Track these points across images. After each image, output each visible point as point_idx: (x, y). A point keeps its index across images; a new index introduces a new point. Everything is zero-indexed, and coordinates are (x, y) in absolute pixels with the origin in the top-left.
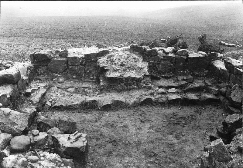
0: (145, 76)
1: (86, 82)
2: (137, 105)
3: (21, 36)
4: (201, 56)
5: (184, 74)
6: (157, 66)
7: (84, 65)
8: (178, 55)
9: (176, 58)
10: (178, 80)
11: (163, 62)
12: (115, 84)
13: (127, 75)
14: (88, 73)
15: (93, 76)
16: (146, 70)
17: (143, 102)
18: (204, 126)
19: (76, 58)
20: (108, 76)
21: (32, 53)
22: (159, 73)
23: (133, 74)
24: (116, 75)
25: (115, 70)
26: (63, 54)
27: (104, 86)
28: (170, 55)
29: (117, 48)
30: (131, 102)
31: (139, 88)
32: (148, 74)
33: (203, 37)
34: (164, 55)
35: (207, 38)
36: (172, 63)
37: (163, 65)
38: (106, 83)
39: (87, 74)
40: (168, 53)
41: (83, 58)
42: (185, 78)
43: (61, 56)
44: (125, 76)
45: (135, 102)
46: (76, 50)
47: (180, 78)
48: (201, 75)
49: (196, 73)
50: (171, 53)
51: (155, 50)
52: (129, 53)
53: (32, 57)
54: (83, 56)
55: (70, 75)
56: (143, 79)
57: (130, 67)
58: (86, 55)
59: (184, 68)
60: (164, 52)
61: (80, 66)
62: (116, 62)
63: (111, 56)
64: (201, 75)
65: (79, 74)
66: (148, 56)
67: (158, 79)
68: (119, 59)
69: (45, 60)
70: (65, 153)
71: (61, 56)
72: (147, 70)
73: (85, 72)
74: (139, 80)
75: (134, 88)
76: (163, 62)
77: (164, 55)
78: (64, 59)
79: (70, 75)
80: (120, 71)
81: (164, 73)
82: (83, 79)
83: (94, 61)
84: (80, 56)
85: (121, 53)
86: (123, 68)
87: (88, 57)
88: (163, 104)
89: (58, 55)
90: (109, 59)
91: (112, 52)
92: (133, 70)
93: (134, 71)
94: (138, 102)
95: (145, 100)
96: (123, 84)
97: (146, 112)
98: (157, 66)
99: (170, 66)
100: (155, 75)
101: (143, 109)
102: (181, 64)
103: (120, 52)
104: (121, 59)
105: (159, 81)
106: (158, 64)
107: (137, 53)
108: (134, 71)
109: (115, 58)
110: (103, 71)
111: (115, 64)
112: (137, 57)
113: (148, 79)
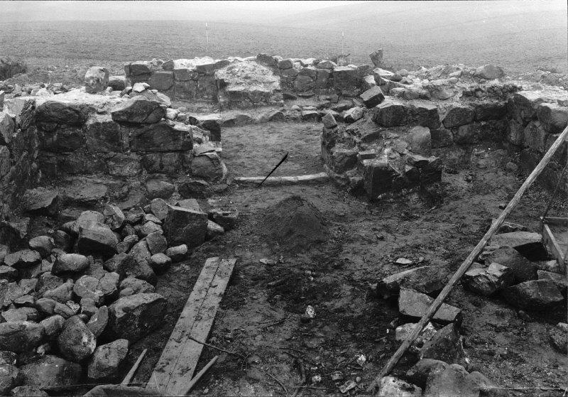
0: (277, 91)
1: (199, 102)
2: (264, 121)
3: (48, 56)
4: (350, 69)
5: (327, 93)
6: (292, 82)
7: (197, 81)
8: (320, 68)
9: (317, 72)
10: (319, 100)
11: (299, 77)
12: (236, 99)
13: (253, 88)
14: (201, 91)
15: (208, 94)
16: (277, 85)
17: (272, 117)
18: (428, 257)
19: (186, 70)
20: (230, 90)
21: (128, 63)
22: (294, 91)
23: (261, 88)
24: (240, 88)
25: (237, 84)
26: (167, 66)
27: (224, 102)
28: (309, 68)
29: (239, 59)
30: (258, 117)
31: (269, 104)
32: (279, 88)
33: (377, 54)
34: (302, 67)
35: (385, 55)
36: (312, 78)
37: (301, 81)
38: (227, 100)
39: (201, 93)
40: (307, 65)
41: (194, 71)
42: (328, 97)
43: (165, 68)
44: (251, 90)
45: (263, 117)
46: (185, 61)
47: (322, 97)
48: (351, 95)
49: (344, 92)
50: (312, 65)
51: (289, 62)
52: (255, 64)
53: (128, 70)
54: (195, 68)
55: (177, 94)
56: (273, 95)
57: (256, 81)
58: (199, 67)
59: (328, 85)
60: (302, 64)
61: (191, 82)
62: (239, 74)
63: (232, 68)
64: (351, 95)
65: (190, 93)
66: (280, 69)
67: (293, 98)
68: (243, 71)
69: (143, 74)
70: (204, 125)
71: (165, 68)
72: (278, 84)
73: (197, 89)
74: (267, 96)
75: (262, 105)
76: (299, 77)
77: (302, 67)
78: (170, 73)
79: (177, 94)
80: (244, 84)
81: (302, 91)
82: (195, 99)
83: (209, 75)
84: (190, 69)
85: (244, 65)
86: (248, 81)
87: (201, 70)
88: (295, 119)
89: (160, 67)
90: (230, 71)
91: (233, 62)
92: (260, 83)
93: (262, 85)
94: (266, 117)
95: (275, 115)
96: (248, 100)
97: (275, 126)
98: (292, 82)
99: (310, 82)
100: (289, 93)
101: (272, 124)
102: (324, 80)
103: (245, 65)
104: (246, 72)
105: (295, 101)
106: (294, 80)
107: (266, 64)
108: (262, 85)
109: (237, 70)
110: (223, 84)
111: (238, 77)
112: (265, 69)
113: (280, 95)
